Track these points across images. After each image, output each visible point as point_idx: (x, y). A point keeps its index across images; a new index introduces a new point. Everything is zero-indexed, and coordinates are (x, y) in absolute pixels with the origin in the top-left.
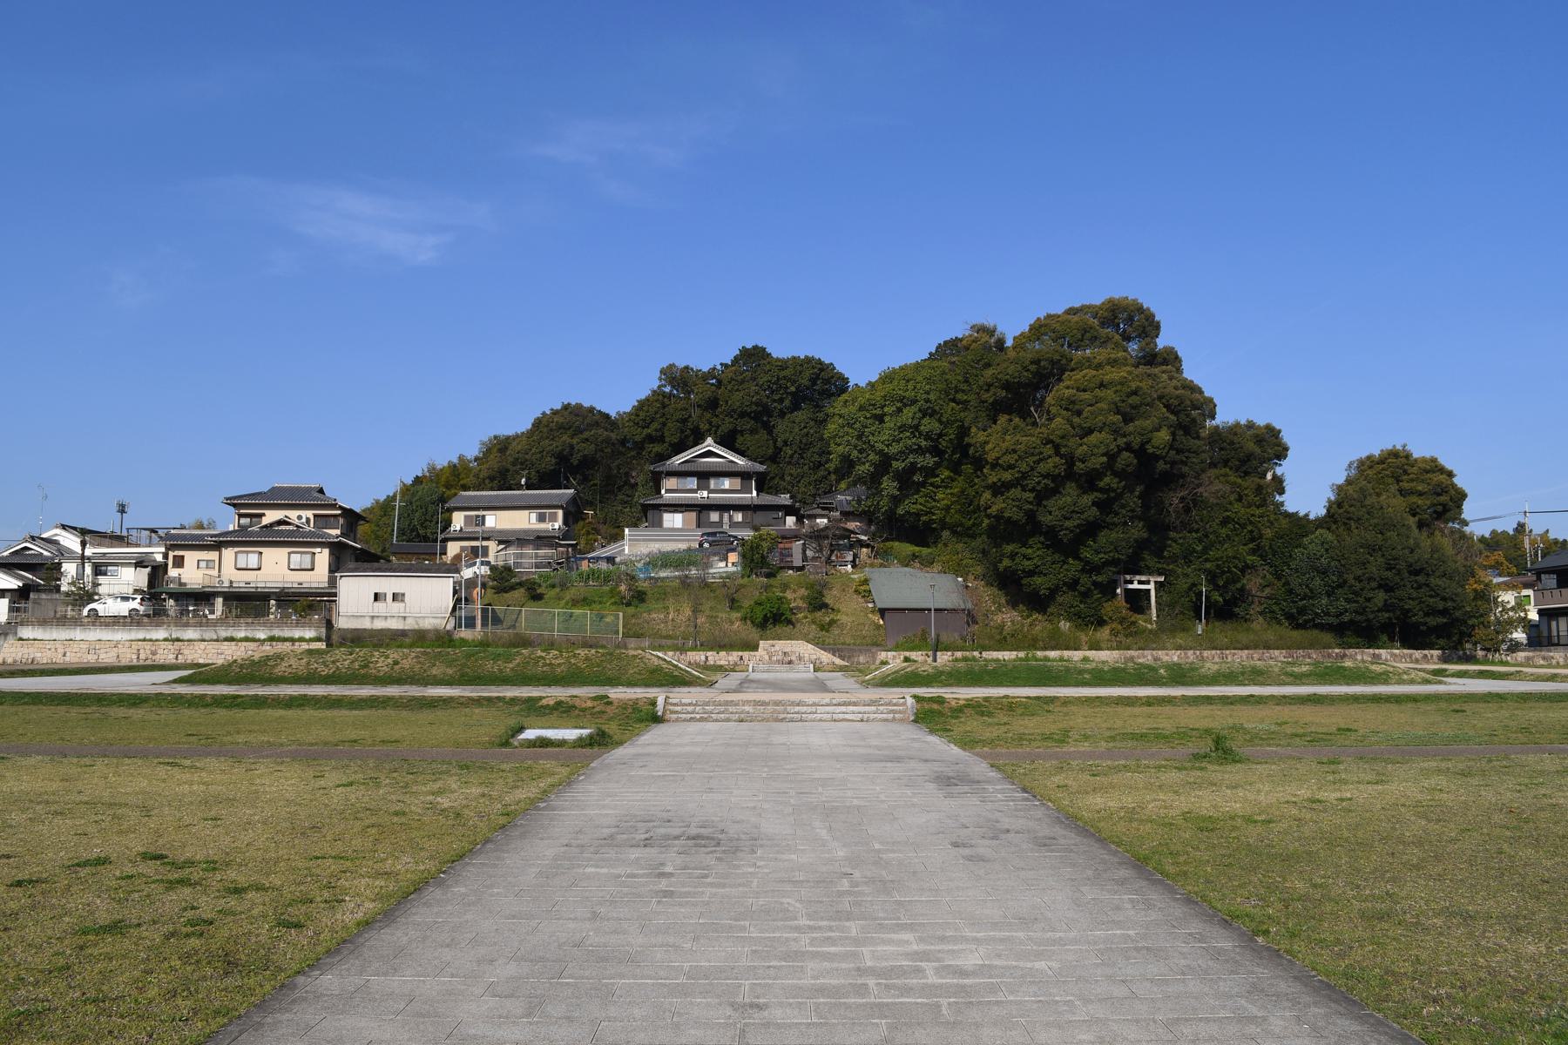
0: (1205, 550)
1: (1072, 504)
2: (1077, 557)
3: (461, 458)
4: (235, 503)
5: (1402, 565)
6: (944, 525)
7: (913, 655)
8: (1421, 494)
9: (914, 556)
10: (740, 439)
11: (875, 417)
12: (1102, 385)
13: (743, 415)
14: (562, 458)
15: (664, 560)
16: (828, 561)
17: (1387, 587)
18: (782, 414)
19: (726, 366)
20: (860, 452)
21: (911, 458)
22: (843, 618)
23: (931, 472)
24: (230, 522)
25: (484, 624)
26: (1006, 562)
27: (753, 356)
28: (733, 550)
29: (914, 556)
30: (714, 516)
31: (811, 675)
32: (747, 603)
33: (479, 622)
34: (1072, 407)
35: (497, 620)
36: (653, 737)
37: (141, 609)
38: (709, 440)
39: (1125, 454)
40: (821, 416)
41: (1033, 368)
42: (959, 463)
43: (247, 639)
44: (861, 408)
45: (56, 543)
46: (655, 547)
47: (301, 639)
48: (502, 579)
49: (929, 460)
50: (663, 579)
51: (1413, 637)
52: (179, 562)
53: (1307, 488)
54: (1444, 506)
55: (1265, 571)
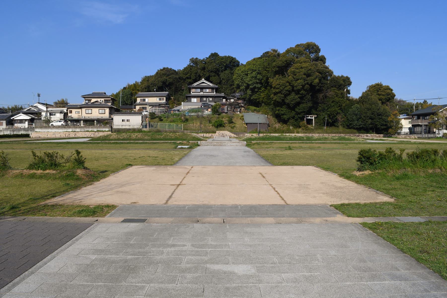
0: (328, 109)
1: (293, 98)
2: (294, 111)
3: (136, 82)
4: (84, 97)
5: (375, 113)
6: (263, 102)
7: (254, 134)
8: (383, 95)
9: (255, 110)
10: (211, 78)
11: (245, 74)
12: (302, 68)
13: (212, 72)
14: (164, 83)
15: (192, 110)
16: (234, 111)
17: (371, 118)
18: (222, 71)
19: (207, 58)
20: (242, 83)
21: (254, 85)
22: (237, 125)
23: (259, 89)
24: (83, 102)
25: (149, 127)
26: (277, 112)
27: (214, 56)
28: (210, 108)
29: (255, 110)
30: (205, 99)
31: (229, 139)
32: (213, 122)
33: (148, 126)
34: (294, 73)
35: (152, 126)
36: (199, 147)
37: (64, 124)
38: (203, 79)
39: (307, 85)
40: (232, 72)
41: (285, 62)
42: (267, 86)
43: (92, 131)
44: (242, 72)
45: (37, 107)
46: (190, 107)
47: (105, 131)
48: (152, 116)
49: (259, 86)
50: (192, 116)
51: (378, 131)
52: (71, 112)
53: (356, 92)
54: (389, 98)
55: (343, 114)
